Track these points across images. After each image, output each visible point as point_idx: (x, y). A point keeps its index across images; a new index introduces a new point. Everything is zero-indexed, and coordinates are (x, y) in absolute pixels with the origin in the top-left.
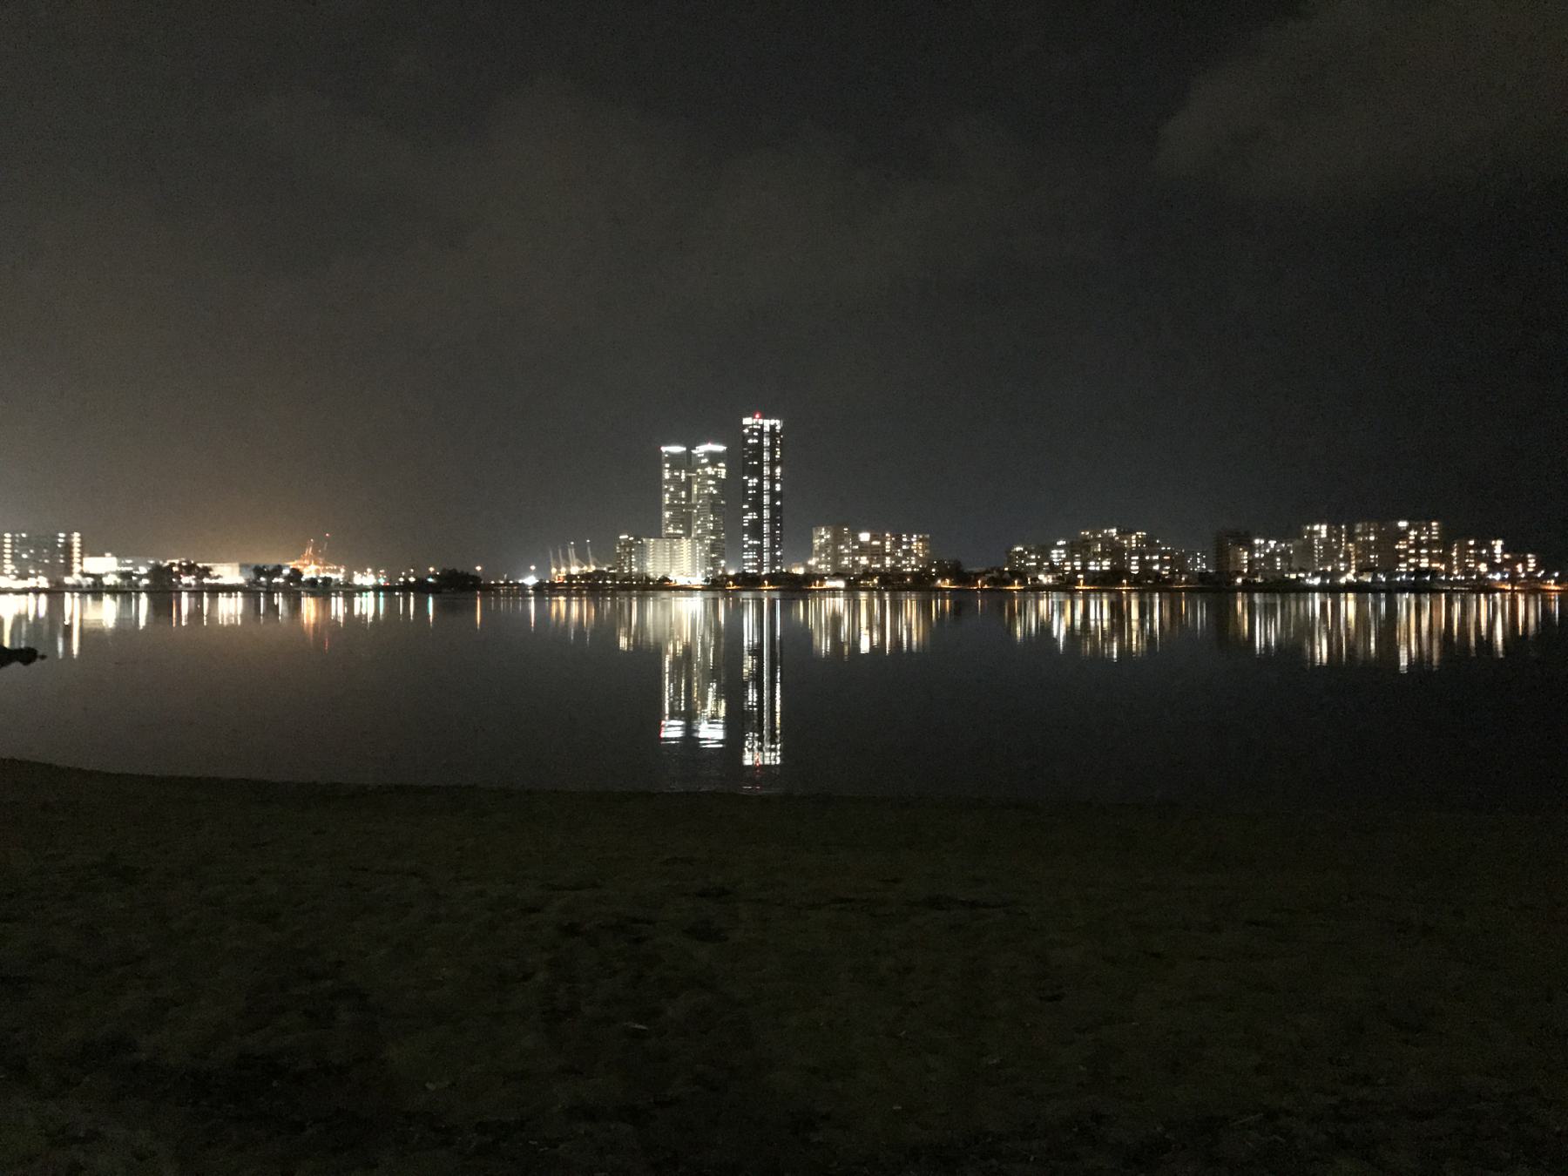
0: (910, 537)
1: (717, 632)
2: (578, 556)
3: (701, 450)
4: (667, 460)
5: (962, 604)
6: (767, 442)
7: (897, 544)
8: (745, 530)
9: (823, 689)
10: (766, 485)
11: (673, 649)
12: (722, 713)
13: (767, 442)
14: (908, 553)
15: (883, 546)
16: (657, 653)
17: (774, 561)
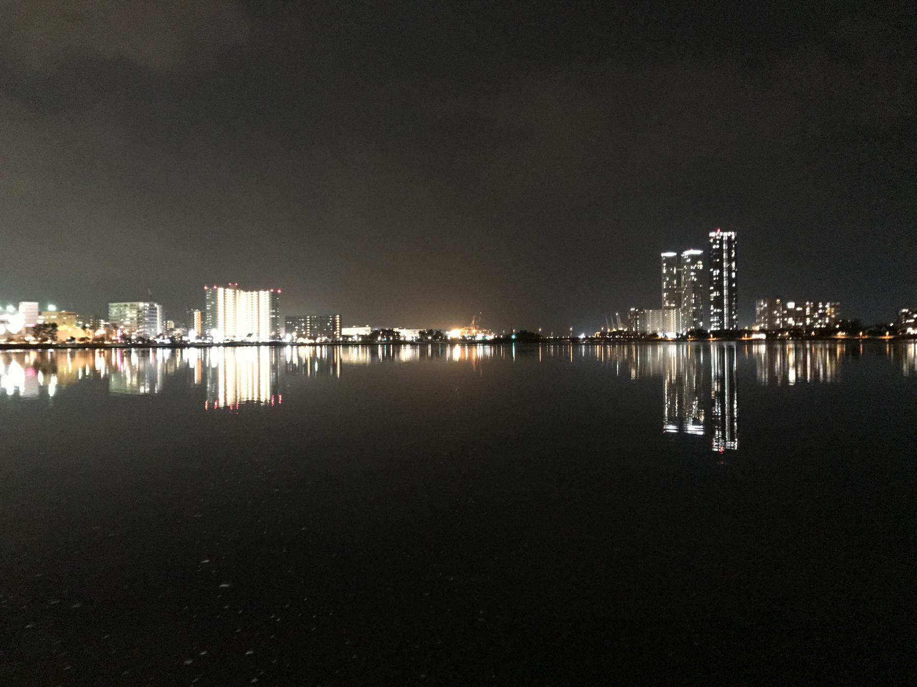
0: (824, 304)
1: (698, 367)
2: (622, 321)
3: (686, 253)
5: (851, 345)
6: (725, 247)
7: (815, 309)
8: (711, 303)
9: (761, 401)
10: (725, 274)
11: (671, 376)
12: (702, 419)
13: (725, 247)
14: (823, 316)
15: (804, 311)
16: (658, 379)
17: (731, 322)
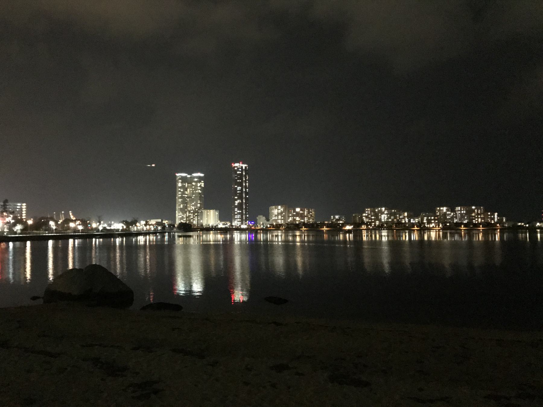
4: (180, 179)
8: (236, 207)
